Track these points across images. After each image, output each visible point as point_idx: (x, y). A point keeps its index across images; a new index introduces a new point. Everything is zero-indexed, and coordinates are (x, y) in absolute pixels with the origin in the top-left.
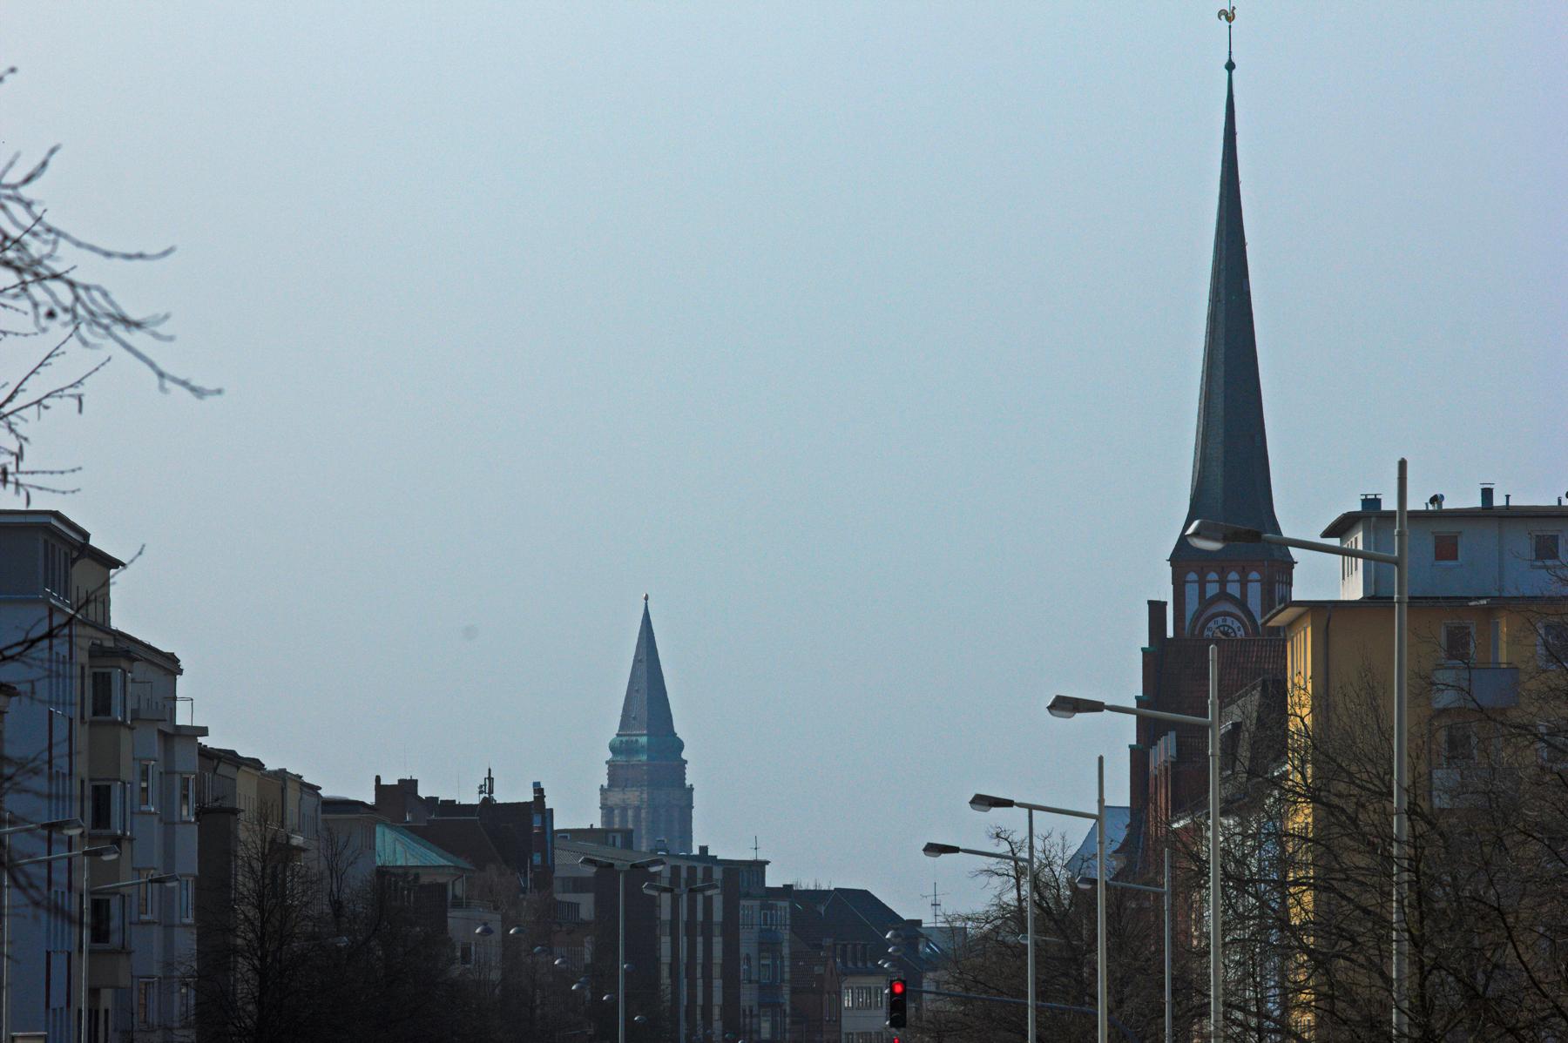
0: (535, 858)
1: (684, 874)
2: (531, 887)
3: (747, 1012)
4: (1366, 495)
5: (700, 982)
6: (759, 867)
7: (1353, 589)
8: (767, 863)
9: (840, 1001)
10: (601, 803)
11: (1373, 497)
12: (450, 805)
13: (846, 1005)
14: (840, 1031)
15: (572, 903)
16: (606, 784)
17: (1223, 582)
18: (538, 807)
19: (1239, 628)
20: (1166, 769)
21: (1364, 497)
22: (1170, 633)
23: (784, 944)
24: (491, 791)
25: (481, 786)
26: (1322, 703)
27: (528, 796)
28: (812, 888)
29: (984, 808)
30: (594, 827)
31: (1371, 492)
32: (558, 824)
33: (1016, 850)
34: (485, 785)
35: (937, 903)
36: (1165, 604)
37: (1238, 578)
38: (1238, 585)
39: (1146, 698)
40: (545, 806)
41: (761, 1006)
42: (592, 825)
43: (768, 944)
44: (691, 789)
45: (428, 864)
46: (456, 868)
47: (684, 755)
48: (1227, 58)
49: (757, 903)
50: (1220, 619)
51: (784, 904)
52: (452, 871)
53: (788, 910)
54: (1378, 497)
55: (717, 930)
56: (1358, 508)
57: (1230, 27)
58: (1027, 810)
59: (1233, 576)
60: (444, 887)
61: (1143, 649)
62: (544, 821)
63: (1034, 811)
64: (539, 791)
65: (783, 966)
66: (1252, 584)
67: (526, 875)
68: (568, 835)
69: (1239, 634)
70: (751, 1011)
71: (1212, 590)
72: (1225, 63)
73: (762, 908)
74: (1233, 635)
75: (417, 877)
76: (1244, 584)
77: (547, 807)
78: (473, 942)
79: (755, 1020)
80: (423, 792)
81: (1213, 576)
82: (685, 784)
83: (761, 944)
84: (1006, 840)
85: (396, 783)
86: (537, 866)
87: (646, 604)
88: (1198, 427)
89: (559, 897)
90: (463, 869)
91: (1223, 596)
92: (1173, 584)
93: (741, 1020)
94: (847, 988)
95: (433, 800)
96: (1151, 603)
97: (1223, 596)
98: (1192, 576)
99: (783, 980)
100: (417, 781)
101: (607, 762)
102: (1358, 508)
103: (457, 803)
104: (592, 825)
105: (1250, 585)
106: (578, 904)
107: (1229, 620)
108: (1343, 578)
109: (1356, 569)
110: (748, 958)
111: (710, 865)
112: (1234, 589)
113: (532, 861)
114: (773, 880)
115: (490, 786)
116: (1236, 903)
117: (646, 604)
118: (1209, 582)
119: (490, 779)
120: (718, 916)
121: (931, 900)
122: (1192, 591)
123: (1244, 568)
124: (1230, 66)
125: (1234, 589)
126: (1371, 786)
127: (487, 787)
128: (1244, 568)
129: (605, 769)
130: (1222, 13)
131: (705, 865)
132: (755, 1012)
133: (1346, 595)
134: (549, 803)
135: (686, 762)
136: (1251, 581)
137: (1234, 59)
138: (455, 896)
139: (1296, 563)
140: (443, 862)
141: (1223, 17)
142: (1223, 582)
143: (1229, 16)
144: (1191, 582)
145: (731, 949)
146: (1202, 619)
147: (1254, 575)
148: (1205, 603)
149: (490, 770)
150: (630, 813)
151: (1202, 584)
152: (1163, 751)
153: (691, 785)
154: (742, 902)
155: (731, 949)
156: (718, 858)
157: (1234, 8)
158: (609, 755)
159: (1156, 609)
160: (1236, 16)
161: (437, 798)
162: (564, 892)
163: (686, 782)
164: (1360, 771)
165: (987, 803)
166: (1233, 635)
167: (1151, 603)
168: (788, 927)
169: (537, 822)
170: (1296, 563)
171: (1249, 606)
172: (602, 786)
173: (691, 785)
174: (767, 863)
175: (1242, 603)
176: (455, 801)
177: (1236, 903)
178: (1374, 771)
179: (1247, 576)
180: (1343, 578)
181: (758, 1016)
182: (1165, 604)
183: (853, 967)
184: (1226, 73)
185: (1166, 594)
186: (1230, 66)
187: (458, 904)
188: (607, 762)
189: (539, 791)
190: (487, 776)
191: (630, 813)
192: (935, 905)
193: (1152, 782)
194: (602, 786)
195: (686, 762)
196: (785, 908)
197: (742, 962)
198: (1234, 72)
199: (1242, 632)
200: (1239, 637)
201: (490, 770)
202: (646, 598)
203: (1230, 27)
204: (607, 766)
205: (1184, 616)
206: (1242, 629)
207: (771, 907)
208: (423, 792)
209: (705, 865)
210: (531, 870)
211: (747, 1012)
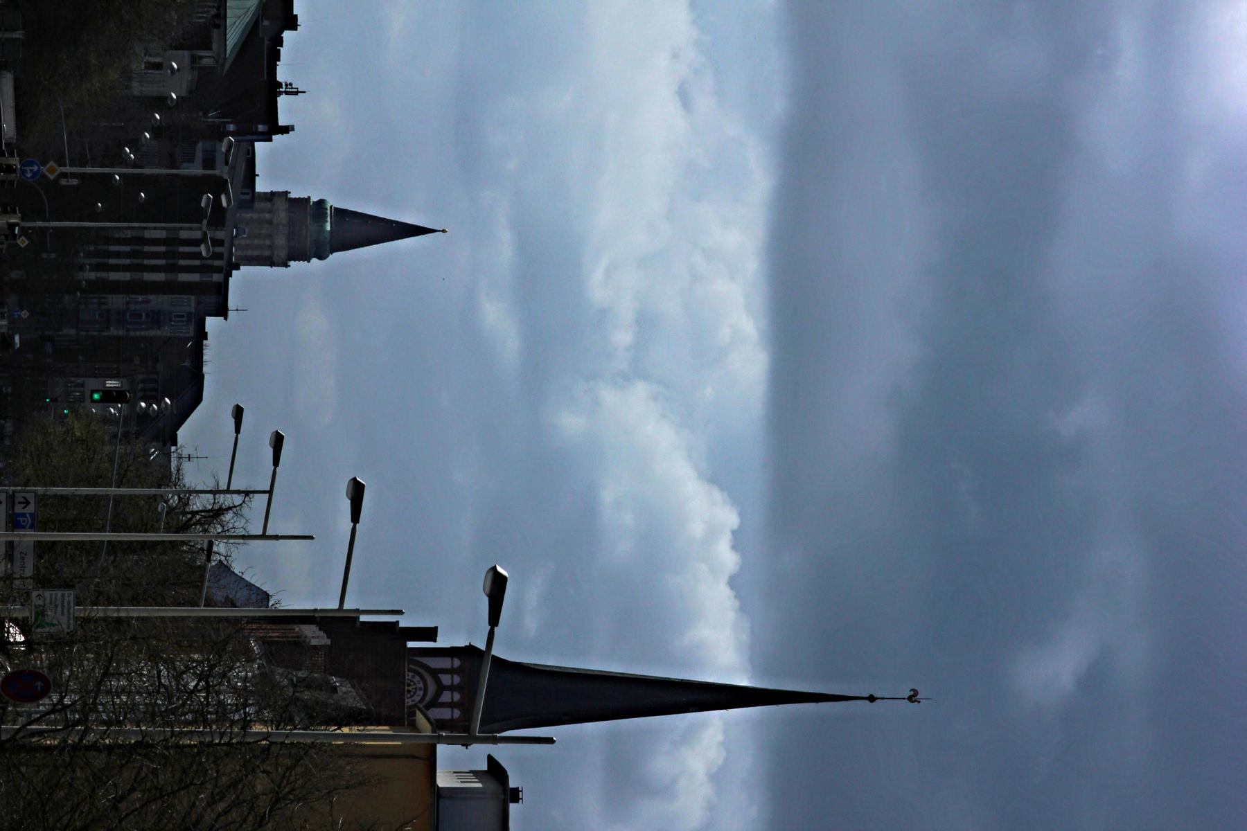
2: (207, 122)
3: (102, 300)
4: (522, 791)
6: (222, 310)
7: (444, 780)
8: (226, 319)
9: (111, 377)
10: (275, 192)
11: (521, 797)
12: (276, 56)
13: (107, 382)
14: (86, 376)
15: (194, 156)
16: (292, 196)
17: (452, 688)
18: (275, 129)
19: (413, 701)
20: (298, 637)
21: (520, 789)
22: (411, 644)
23: (158, 331)
24: (287, 93)
25: (291, 84)
26: (350, 752)
27: (282, 122)
28: (205, 358)
29: (273, 442)
31: (525, 795)
32: (259, 146)
33: (234, 510)
34: (292, 88)
35: (191, 459)
37: (454, 717)
38: (450, 701)
39: (358, 624)
40: (275, 134)
42: (258, 175)
43: (156, 318)
44: (287, 266)
45: (228, 37)
47: (314, 260)
48: (878, 696)
49: (193, 310)
50: (421, 685)
51: (191, 331)
52: (222, 55)
53: (187, 335)
54: (521, 800)
55: (170, 276)
56: (512, 784)
57: (904, 699)
59: (457, 697)
60: (209, 48)
62: (262, 133)
63: (267, 495)
64: (286, 130)
66: (450, 696)
67: (217, 118)
68: (250, 156)
69: (410, 700)
70: (103, 303)
71: (446, 679)
72: (874, 695)
73: (189, 314)
74: (409, 695)
75: (218, 26)
76: (451, 705)
78: (162, 72)
80: (287, 35)
81: (457, 679)
83: (159, 312)
84: (244, 502)
85: (294, 13)
86: (225, 127)
87: (439, 231)
89: (200, 146)
90: (223, 66)
91: (441, 688)
92: (451, 648)
94: (122, 384)
95: (280, 42)
96: (436, 628)
97: (441, 688)
99: (128, 330)
100: (296, 30)
102: (512, 784)
103: (278, 63)
104: (258, 175)
105: (450, 659)
106: (193, 162)
107: (421, 693)
108: (454, 772)
109: (462, 782)
110: (149, 302)
111: (224, 271)
112: (446, 697)
113: (229, 123)
114: (211, 323)
115: (292, 92)
116: (190, 672)
117: (439, 231)
118: (452, 677)
119: (297, 93)
120: (183, 277)
121: (193, 454)
122: (444, 663)
124: (872, 699)
125: (446, 697)
126: (285, 782)
127: (291, 90)
130: (915, 693)
132: (103, 307)
133: (441, 774)
135: (309, 262)
136: (452, 677)
138: (201, 57)
139: (467, 748)
140: (229, 48)
141: (912, 693)
142: (452, 688)
144: (452, 663)
145: (157, 288)
146: (421, 671)
147: (457, 713)
148: (435, 673)
149: (304, 92)
152: (313, 635)
153: (289, 266)
154: (193, 298)
155: (157, 288)
156: (230, 278)
157: (919, 702)
158: (314, 199)
159: (431, 634)
160: (916, 688)
161: (282, 46)
162: (203, 151)
163: (293, 262)
164: (296, 775)
165: (269, 263)
166: (409, 695)
167: (436, 628)
168: (172, 335)
170: (467, 748)
171: (432, 709)
172: (290, 193)
173: (289, 266)
174: (226, 319)
175: (434, 703)
176: (279, 61)
177: (190, 672)
178: (297, 786)
179: (457, 708)
180: (454, 772)
183: (139, 388)
184: (867, 695)
185: (442, 642)
186: (872, 699)
187: (195, 59)
189: (286, 130)
190: (299, 90)
191: (267, 216)
192: (189, 458)
193: (290, 626)
194: (290, 193)
195: (309, 262)
196: (189, 333)
197: (143, 297)
198: (867, 702)
199: (411, 703)
200: (407, 701)
201: (304, 92)
202: (444, 231)
203: (904, 699)
204: (306, 197)
205: (425, 656)
206: (414, 703)
207: (189, 320)
208: (287, 35)
209: (225, 267)
210: (222, 122)
211: (102, 300)
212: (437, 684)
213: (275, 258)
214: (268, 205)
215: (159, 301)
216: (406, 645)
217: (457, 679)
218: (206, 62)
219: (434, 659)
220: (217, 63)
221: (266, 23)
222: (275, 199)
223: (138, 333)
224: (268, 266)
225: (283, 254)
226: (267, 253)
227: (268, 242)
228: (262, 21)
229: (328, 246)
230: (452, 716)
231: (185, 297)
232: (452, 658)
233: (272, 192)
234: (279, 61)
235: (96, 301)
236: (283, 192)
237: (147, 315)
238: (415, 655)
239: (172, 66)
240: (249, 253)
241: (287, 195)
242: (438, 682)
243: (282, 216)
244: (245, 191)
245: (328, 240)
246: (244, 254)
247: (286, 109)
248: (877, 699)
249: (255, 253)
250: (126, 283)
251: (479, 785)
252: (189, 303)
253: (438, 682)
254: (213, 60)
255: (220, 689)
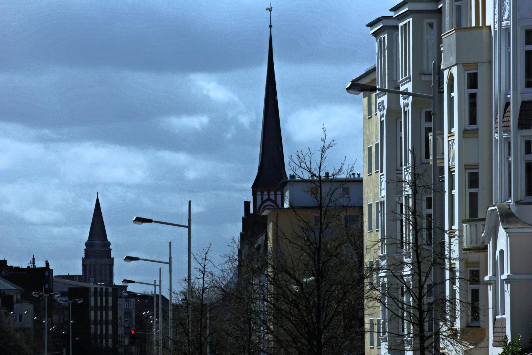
0: (46, 286)
1: (99, 290)
5: (404, 232)
12: (17, 268)
16: (84, 257)
17: (269, 195)
22: (252, 212)
24: (34, 263)
25: (31, 261)
27: (43, 265)
30: (69, 274)
32: (55, 274)
36: (249, 202)
41: (125, 334)
43: (128, 314)
44: (113, 259)
46: (18, 290)
47: (111, 247)
52: (16, 291)
53: (134, 302)
58: (154, 286)
59: (272, 193)
61: (243, 217)
62: (49, 273)
65: (132, 320)
68: (60, 277)
70: (122, 335)
71: (265, 197)
75: (4, 293)
76: (276, 195)
77: (50, 269)
79: (123, 339)
80: (9, 264)
82: (111, 257)
83: (125, 313)
88: (261, 144)
90: (21, 290)
92: (253, 195)
93: (118, 338)
95: (12, 267)
97: (269, 199)
98: (259, 193)
100: (6, 261)
101: (84, 250)
105: (277, 196)
112: (272, 197)
113: (45, 287)
119: (34, 259)
123: (276, 191)
124: (271, 26)
125: (272, 197)
128: (276, 191)
129: (83, 252)
130: (268, 9)
131: (106, 287)
132: (123, 335)
134: (51, 267)
135: (111, 249)
136: (265, 195)
137: (272, 24)
138: (17, 299)
139: (68, 274)
140: (13, 288)
141: (268, 10)
142: (269, 195)
143: (270, 10)
148: (263, 202)
150: (92, 267)
151: (262, 195)
157: (272, 7)
159: (247, 204)
161: (13, 266)
169: (47, 273)
170: (68, 274)
171: (277, 203)
181: (124, 337)
182: (249, 202)
185: (250, 199)
186: (271, 26)
187: (18, 302)
188: (84, 250)
189: (47, 264)
190: (33, 258)
191: (92, 267)
202: (97, 193)
205: (256, 206)
208: (9, 264)
209: (106, 287)
212: (268, 201)
213: (110, 263)
214: (88, 266)
215: (121, 313)
216: (252, 214)
217: (265, 193)
218: (19, 297)
219: (257, 203)
220: (19, 292)
221: (3, 273)
222: (85, 264)
223: (134, 321)
224: (113, 267)
225: (108, 260)
226: (108, 267)
227: (103, 267)
228: (3, 274)
229: (104, 241)
230: (260, 195)
231: (118, 303)
232: (256, 195)
233: (82, 265)
234: (19, 267)
235: (121, 339)
236: (82, 261)
237: (126, 318)
238: (256, 210)
239: (12, 313)
240: (108, 274)
241: (84, 259)
242: (266, 200)
243: (92, 261)
244: (75, 279)
245: (102, 242)
246: (108, 276)
247: (40, 264)
248: (271, 24)
249: (108, 272)
250: (113, 328)
251: (288, 191)
252: (121, 302)
253: (266, 200)
254: (18, 295)
255: (307, 281)
